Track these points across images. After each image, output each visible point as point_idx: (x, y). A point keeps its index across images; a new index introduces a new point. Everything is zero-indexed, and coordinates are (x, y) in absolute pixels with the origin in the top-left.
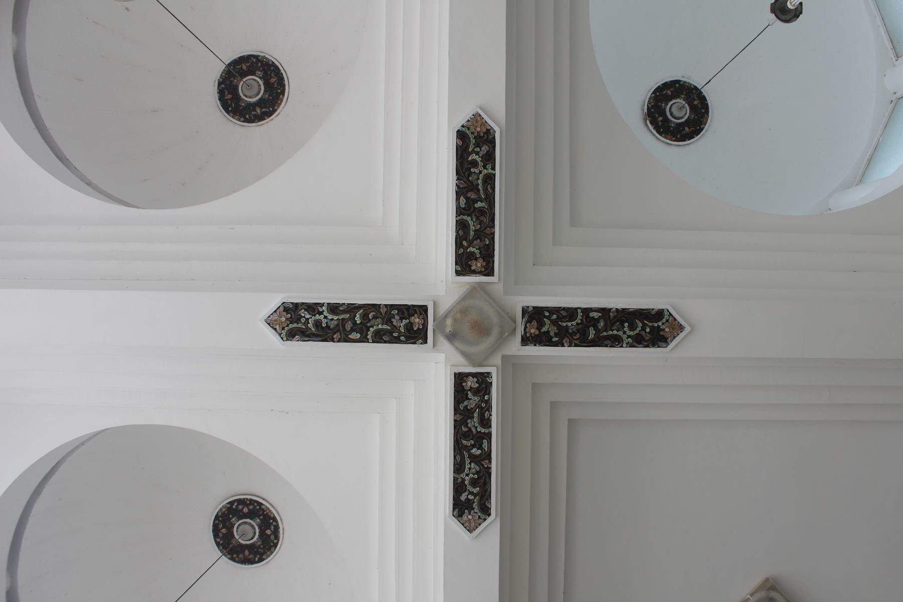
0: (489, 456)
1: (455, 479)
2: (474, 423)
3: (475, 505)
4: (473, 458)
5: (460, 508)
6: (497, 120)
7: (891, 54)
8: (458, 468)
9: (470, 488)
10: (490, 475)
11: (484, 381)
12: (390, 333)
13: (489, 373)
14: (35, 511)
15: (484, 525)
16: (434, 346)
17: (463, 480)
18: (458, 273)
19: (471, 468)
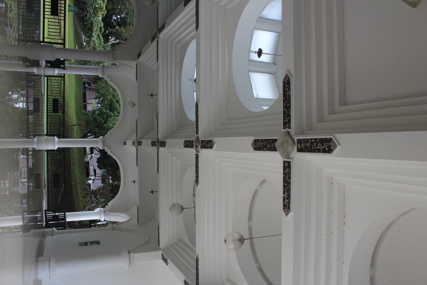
0: (316, 139)
1: (322, 152)
2: (308, 145)
3: (329, 144)
4: (317, 146)
5: (329, 150)
6: (251, 139)
7: (96, 246)
8: (319, 151)
9: (324, 146)
10: (321, 139)
11: (299, 141)
12: (289, 174)
13: (297, 140)
14: (194, 175)
15: (335, 141)
16: (292, 159)
17: (322, 149)
18: (165, 146)
19: (320, 146)
